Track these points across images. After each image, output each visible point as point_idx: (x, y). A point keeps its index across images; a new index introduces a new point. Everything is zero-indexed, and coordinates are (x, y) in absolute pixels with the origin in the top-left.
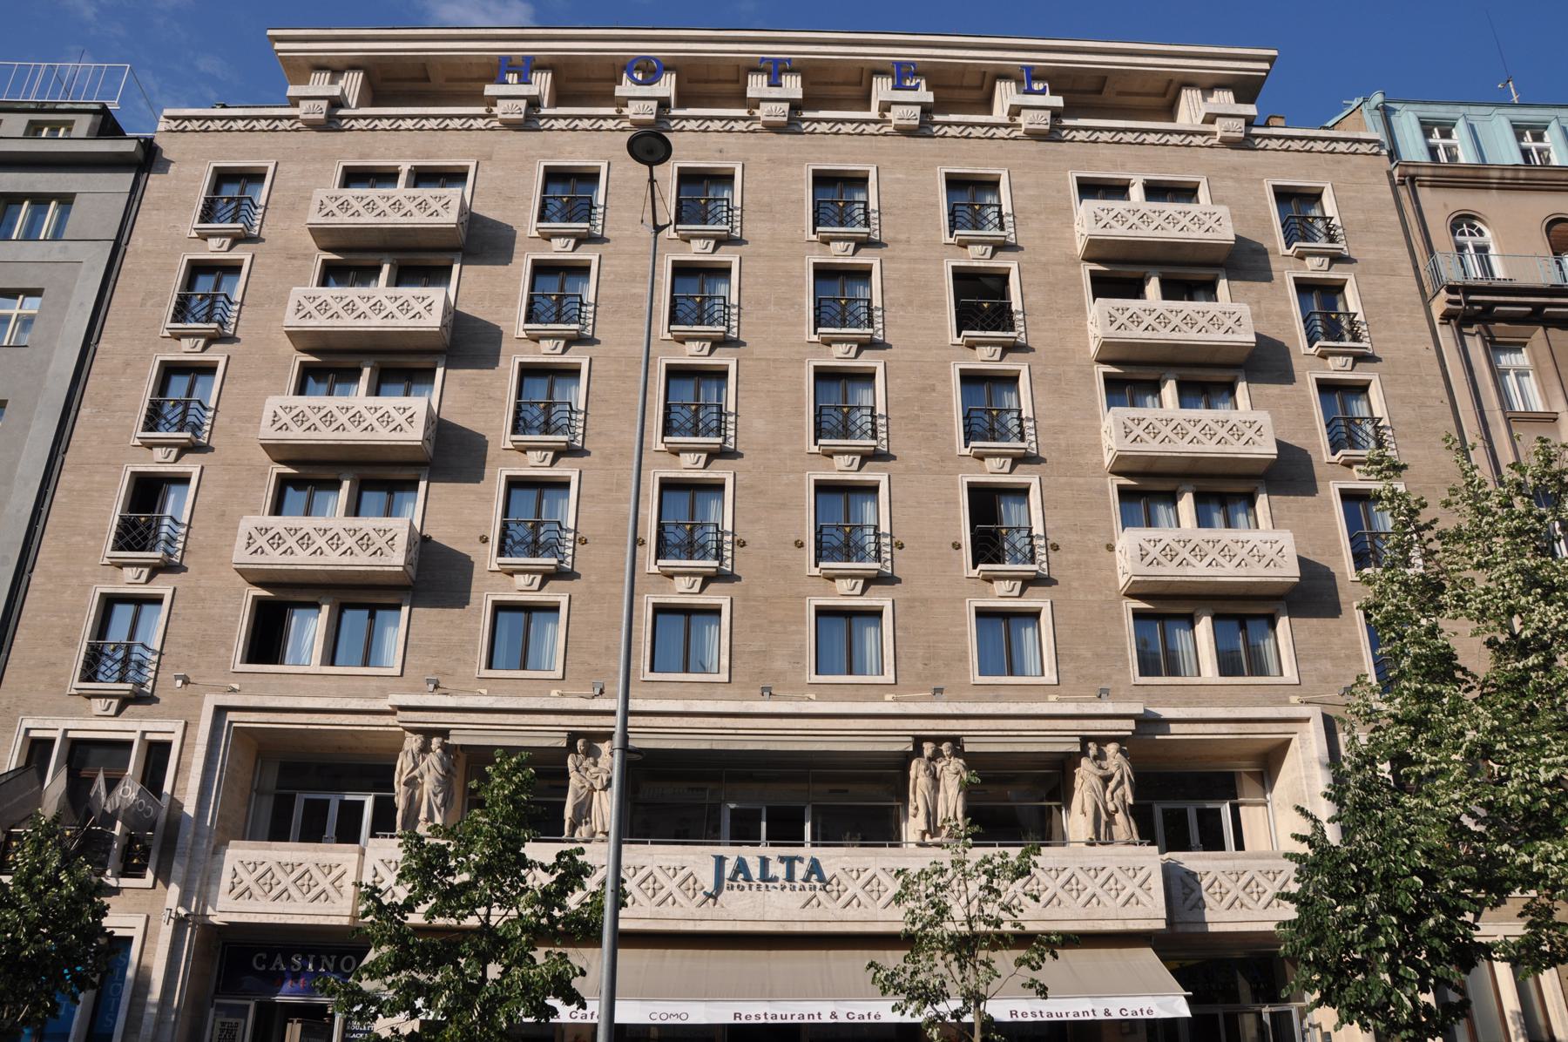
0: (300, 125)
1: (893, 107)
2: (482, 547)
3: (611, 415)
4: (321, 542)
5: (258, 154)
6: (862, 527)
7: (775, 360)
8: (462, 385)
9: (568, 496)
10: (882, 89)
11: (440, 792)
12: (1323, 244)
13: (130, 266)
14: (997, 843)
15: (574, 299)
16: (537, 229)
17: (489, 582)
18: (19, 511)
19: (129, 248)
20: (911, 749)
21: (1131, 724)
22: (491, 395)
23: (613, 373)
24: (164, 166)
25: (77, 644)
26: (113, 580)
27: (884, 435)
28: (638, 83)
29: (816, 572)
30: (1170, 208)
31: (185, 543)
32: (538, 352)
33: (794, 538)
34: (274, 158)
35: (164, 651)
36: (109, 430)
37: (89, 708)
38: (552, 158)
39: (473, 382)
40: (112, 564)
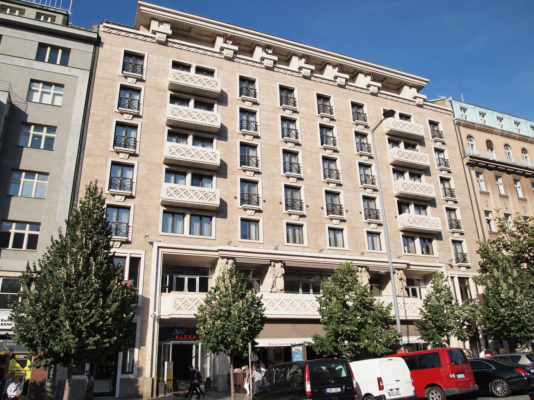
1: (338, 78)
7: (312, 152)
10: (220, 41)
18: (69, 170)
21: (406, 266)
30: (201, 77)
36: (100, 144)
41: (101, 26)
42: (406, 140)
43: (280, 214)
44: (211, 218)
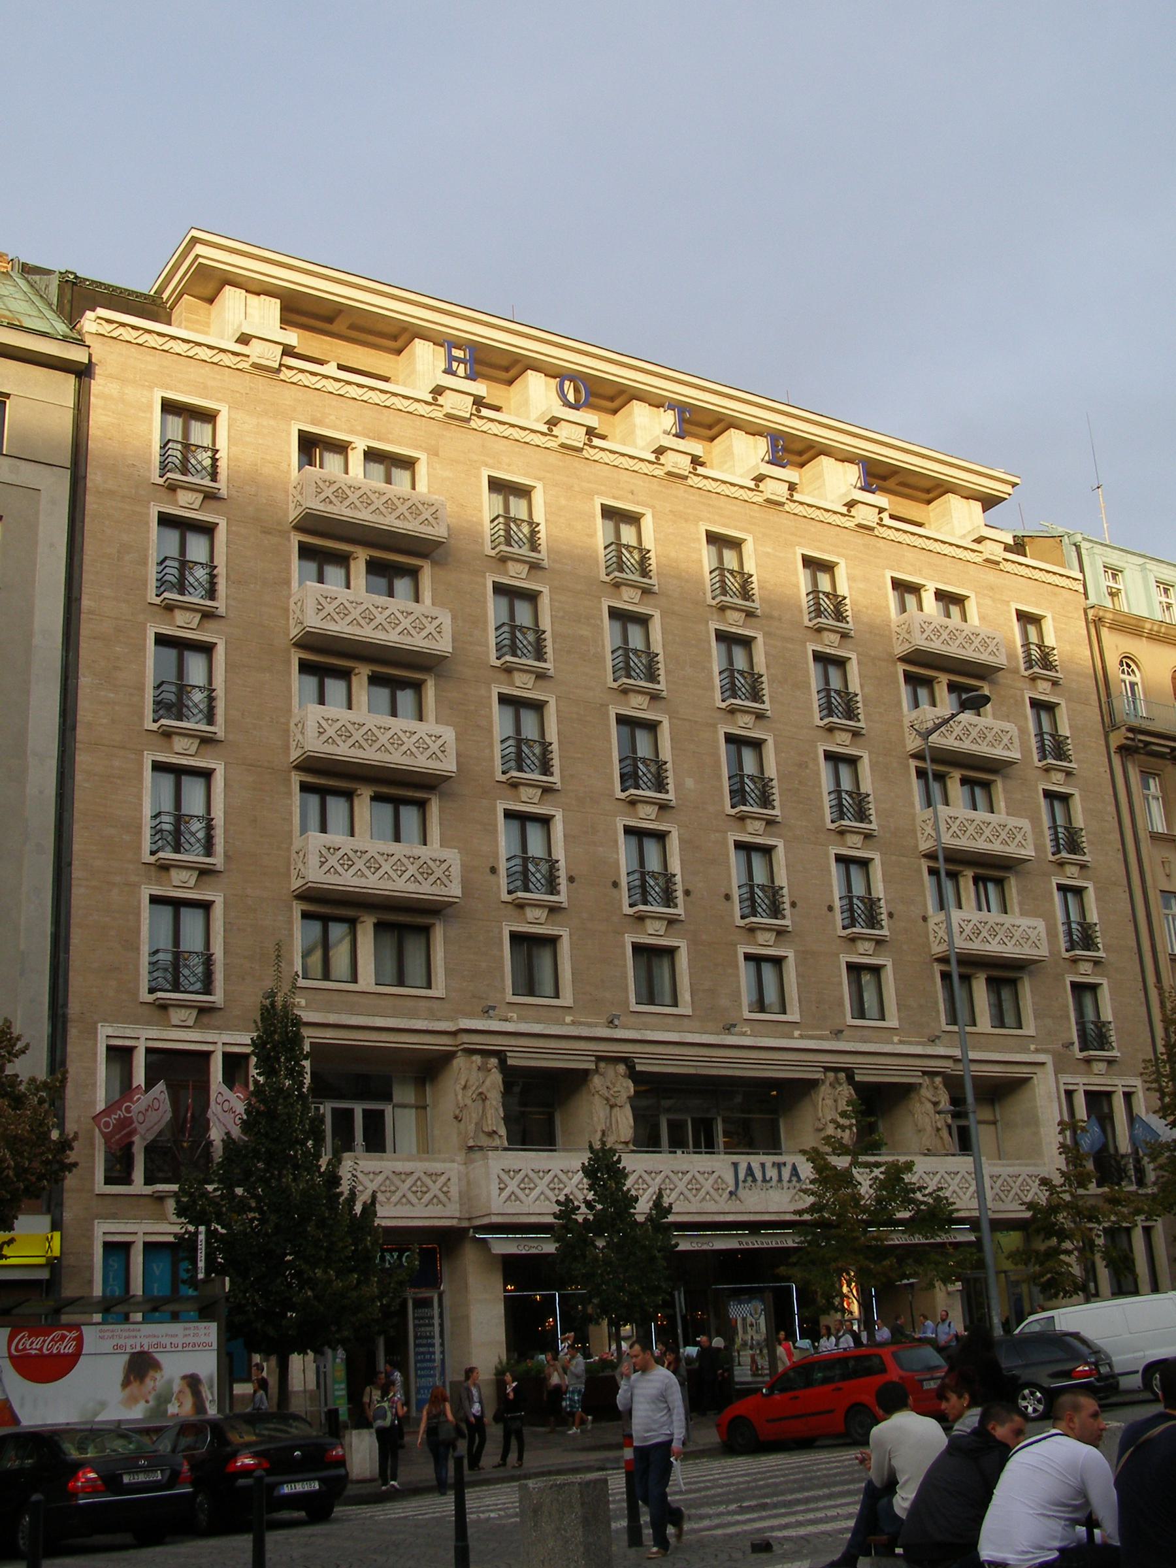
7: (696, 722)
12: (525, 551)
13: (95, 506)
14: (761, 1152)
28: (567, 404)
33: (723, 891)
36: (117, 708)
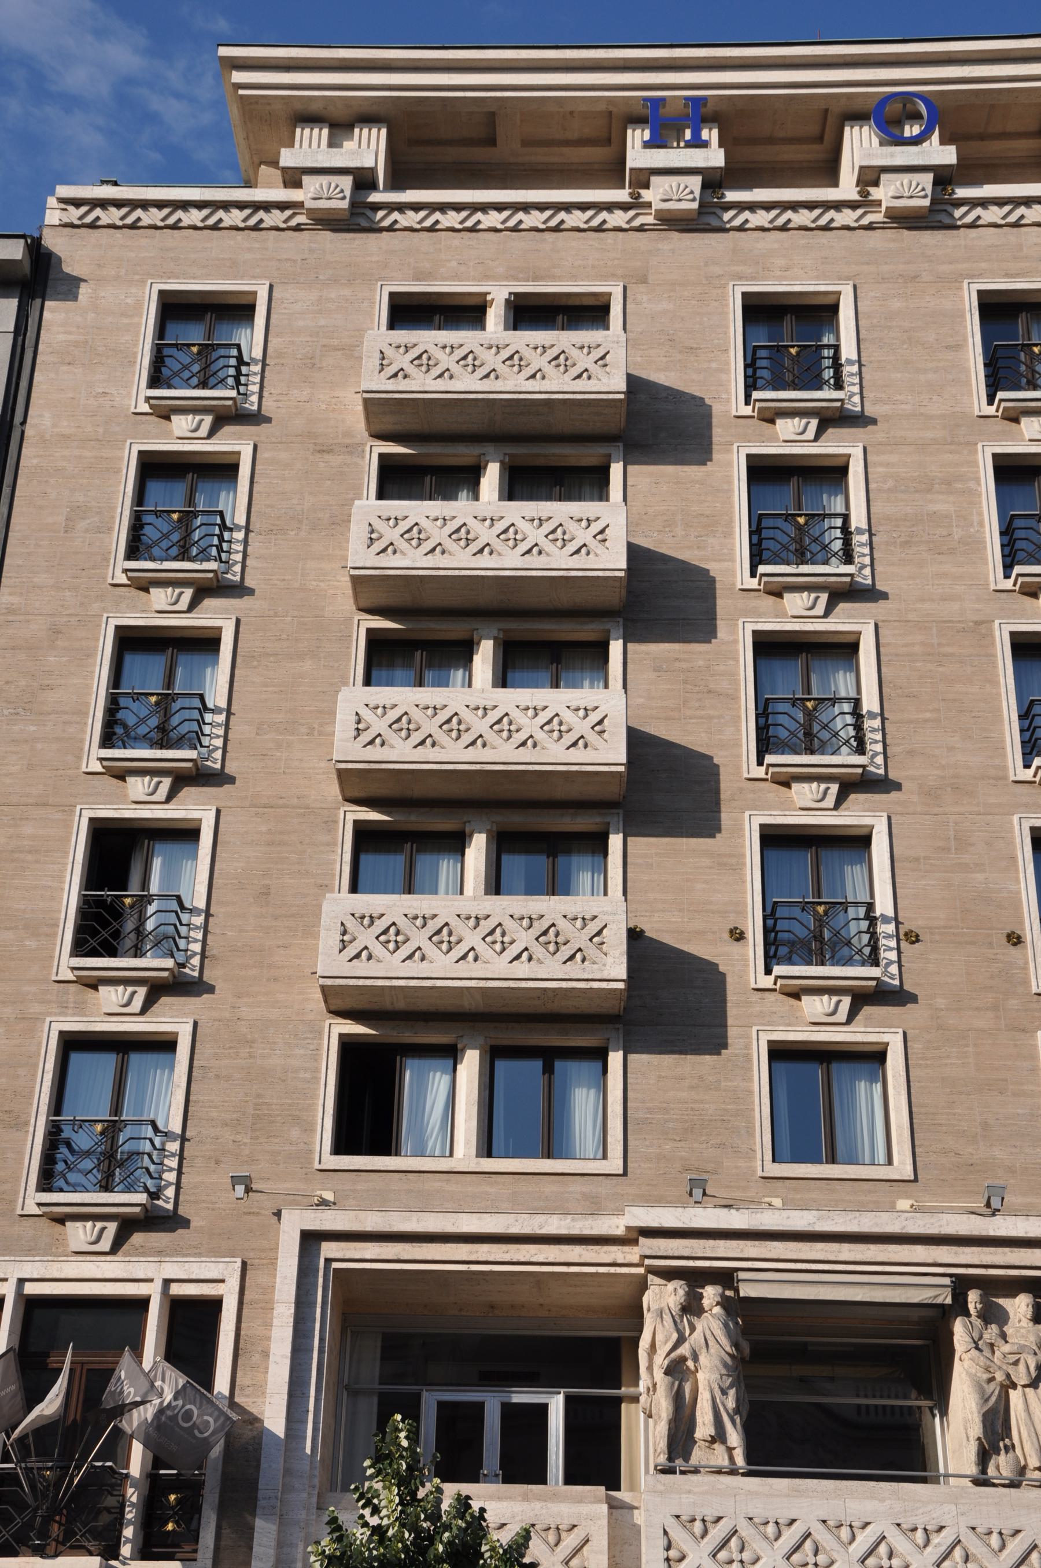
0: (302, 219)
2: (735, 948)
3: (926, 721)
4: (419, 938)
5: (233, 268)
6: (845, 906)
8: (657, 669)
9: (195, 856)
11: (731, 1387)
13: (35, 461)
15: (210, 519)
16: (148, 399)
17: (757, 1009)
19: (29, 431)
20: (949, 1301)
22: (712, 686)
23: (917, 649)
24: (70, 287)
25: (27, 1123)
26: (81, 1009)
27: (879, 748)
29: (767, 982)
31: (204, 941)
32: (782, 614)
34: (266, 278)
35: (188, 1134)
36: (39, 746)
37: (62, 1241)
38: (753, 278)
39: (677, 664)
40: (79, 981)
41: (52, 201)
42: (523, 451)
43: (1013, 1003)
44: (601, 1055)
